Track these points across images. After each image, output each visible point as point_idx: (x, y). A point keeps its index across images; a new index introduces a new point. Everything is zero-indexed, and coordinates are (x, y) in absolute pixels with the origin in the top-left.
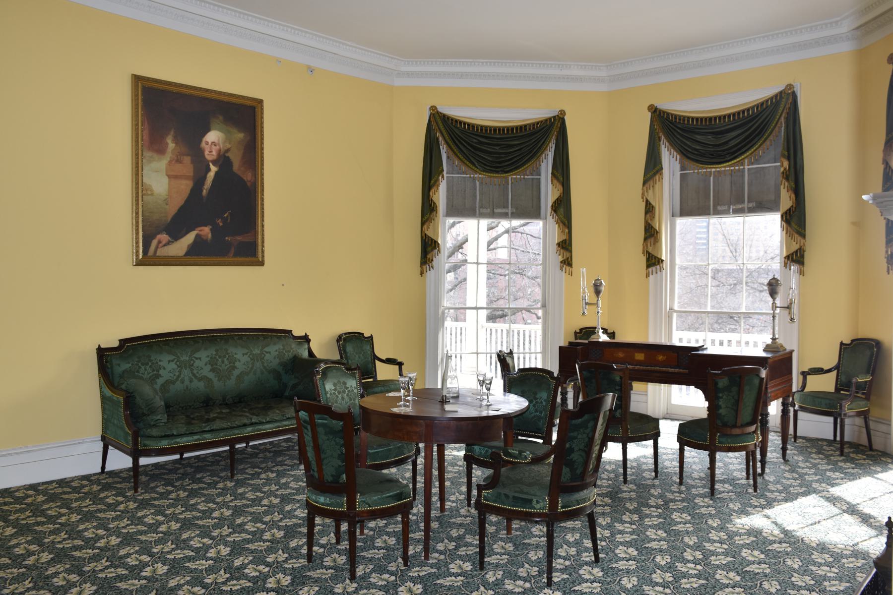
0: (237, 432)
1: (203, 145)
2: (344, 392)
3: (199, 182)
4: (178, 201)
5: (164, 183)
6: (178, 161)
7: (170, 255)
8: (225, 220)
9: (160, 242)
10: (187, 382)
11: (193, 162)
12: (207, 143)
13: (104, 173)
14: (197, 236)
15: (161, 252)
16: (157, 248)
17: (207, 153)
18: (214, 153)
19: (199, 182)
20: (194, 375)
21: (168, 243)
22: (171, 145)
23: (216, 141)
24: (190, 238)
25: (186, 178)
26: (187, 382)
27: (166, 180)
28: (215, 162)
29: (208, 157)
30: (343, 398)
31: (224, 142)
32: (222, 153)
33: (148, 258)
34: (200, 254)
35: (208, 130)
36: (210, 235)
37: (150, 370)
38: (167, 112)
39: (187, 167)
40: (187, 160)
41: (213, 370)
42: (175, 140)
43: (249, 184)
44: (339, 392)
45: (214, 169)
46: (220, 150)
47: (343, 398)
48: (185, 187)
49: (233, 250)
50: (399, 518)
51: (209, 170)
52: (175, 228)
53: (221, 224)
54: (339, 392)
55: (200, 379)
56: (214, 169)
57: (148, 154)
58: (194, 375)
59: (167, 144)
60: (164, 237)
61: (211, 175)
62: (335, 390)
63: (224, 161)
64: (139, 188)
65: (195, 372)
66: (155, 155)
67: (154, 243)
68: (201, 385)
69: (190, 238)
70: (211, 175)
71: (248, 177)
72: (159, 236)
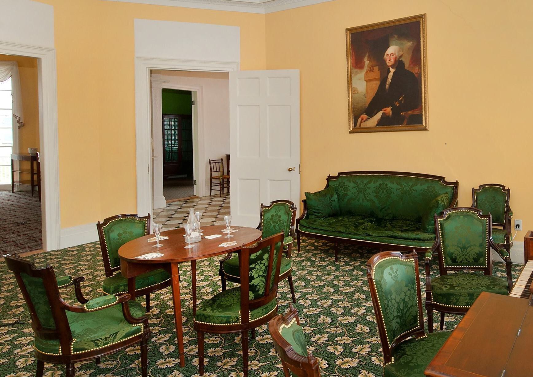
0: (410, 243)
1: (385, 57)
2: (277, 223)
3: (383, 80)
4: (372, 94)
5: (364, 86)
6: (371, 71)
7: (368, 126)
8: (400, 102)
9: (362, 119)
10: (361, 201)
11: (379, 70)
12: (388, 55)
13: (338, 83)
14: (383, 113)
15: (364, 125)
16: (361, 122)
17: (388, 61)
18: (392, 60)
19: (383, 80)
20: (365, 198)
21: (367, 120)
22: (367, 62)
23: (393, 53)
24: (379, 115)
25: (376, 79)
26: (361, 201)
27: (364, 83)
28: (392, 66)
29: (389, 63)
30: (274, 227)
31: (399, 51)
32: (397, 59)
33: (356, 128)
34: (386, 124)
35: (388, 47)
36: (391, 113)
37: (343, 191)
38: (366, 43)
39: (376, 73)
40: (376, 69)
41: (377, 196)
42: (369, 59)
43: (416, 75)
44: (273, 222)
45: (392, 70)
46: (396, 58)
47: (274, 227)
48: (376, 85)
49: (406, 121)
50: (145, 296)
51: (389, 72)
52: (370, 111)
53: (398, 105)
54: (273, 222)
55: (368, 201)
56: (392, 70)
57: (355, 70)
58: (365, 198)
59: (365, 62)
60: (365, 116)
61: (391, 75)
62: (271, 220)
63: (399, 64)
64: (351, 90)
65: (366, 196)
66: (358, 70)
67: (360, 120)
68: (368, 204)
69: (379, 115)
70: (391, 75)
71: (415, 71)
72: (362, 116)
